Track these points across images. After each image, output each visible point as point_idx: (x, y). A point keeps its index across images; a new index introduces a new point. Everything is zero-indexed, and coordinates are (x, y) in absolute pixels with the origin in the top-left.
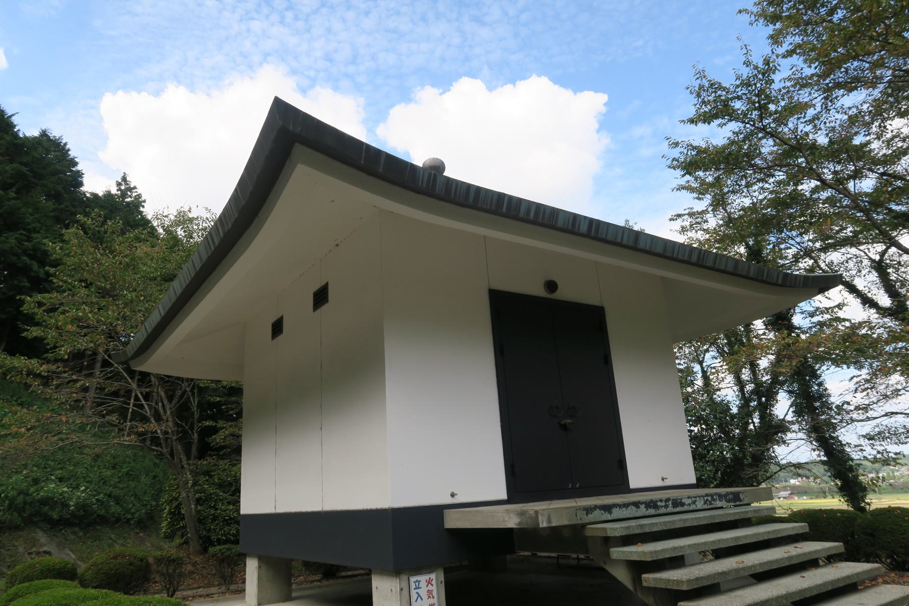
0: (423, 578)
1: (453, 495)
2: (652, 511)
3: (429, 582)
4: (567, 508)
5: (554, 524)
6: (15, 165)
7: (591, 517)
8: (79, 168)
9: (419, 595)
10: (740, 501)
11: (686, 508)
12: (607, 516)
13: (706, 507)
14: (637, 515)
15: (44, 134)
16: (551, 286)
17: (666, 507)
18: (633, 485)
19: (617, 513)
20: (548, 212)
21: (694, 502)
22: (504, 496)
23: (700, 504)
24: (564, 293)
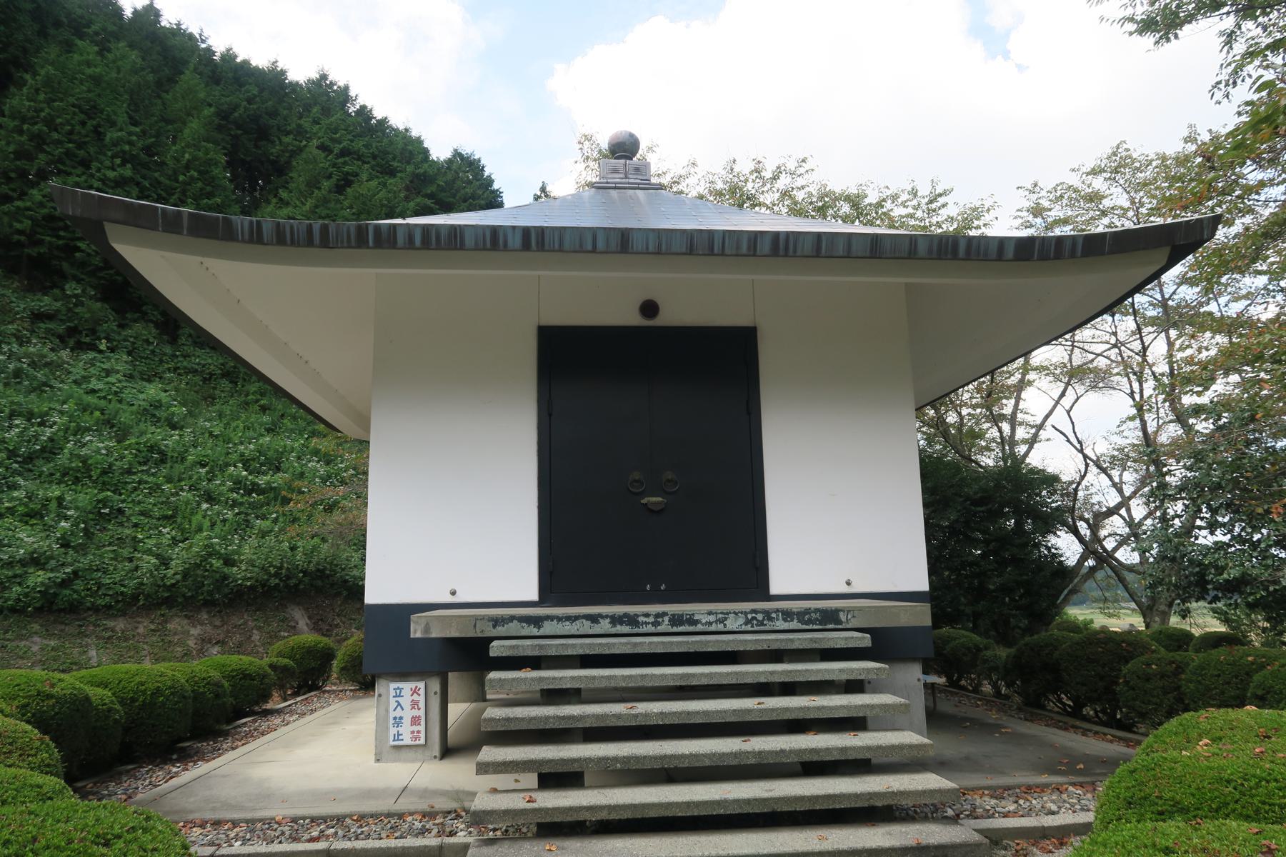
0: (407, 687)
1: (848, 583)
2: (625, 629)
3: (415, 691)
4: (460, 617)
5: (433, 635)
6: (419, 200)
7: (501, 631)
8: (495, 186)
9: (399, 704)
10: (840, 622)
11: (700, 628)
12: (535, 631)
13: (749, 628)
14: (591, 632)
15: (457, 154)
16: (649, 308)
17: (655, 624)
18: (774, 590)
19: (548, 628)
20: (444, 233)
21: (722, 621)
22: (533, 595)
23: (732, 624)
24: (671, 316)
